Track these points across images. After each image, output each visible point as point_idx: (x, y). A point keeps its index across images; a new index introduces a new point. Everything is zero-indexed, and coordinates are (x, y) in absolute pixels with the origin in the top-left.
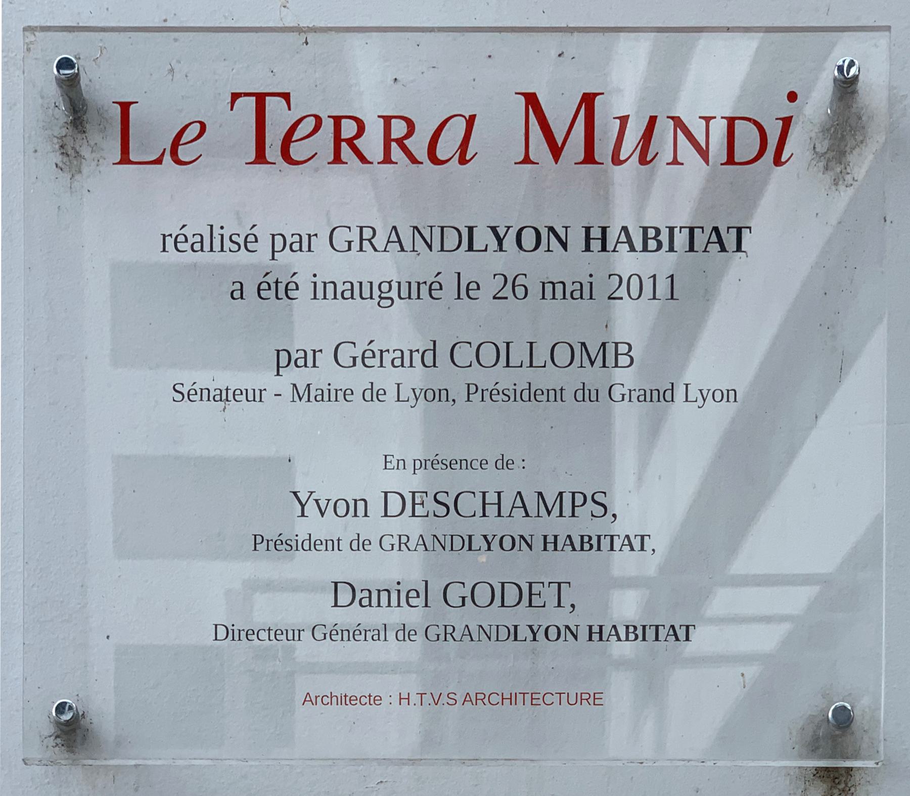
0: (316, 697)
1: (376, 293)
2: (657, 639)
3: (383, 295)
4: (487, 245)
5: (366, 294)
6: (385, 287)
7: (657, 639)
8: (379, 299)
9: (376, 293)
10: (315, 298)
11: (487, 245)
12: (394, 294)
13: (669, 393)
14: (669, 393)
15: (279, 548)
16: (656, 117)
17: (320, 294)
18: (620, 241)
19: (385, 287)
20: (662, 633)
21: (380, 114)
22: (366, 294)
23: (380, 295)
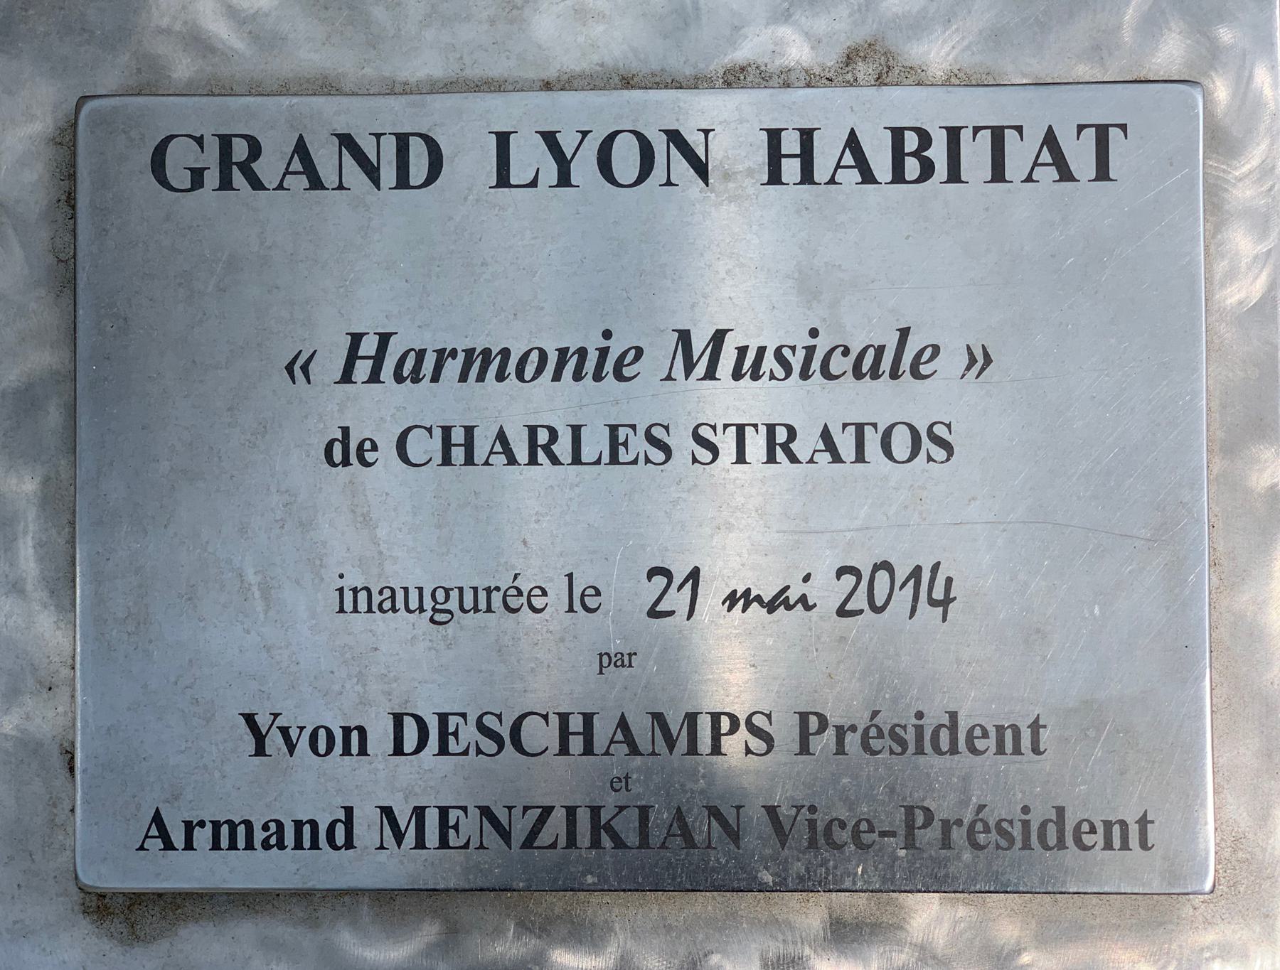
0: (189, 827)
1: (428, 603)
2: (998, 174)
3: (438, 607)
4: (940, 127)
5: (414, 604)
6: (440, 595)
7: (998, 174)
8: (432, 613)
9: (428, 603)
10: (342, 610)
11: (940, 127)
12: (453, 604)
13: (340, 831)
14: (340, 831)
15: (538, 592)
16: (908, 329)
17: (348, 605)
18: (149, 834)
19: (440, 595)
20: (1019, 155)
21: (719, 381)
22: (414, 604)
23: (434, 606)
